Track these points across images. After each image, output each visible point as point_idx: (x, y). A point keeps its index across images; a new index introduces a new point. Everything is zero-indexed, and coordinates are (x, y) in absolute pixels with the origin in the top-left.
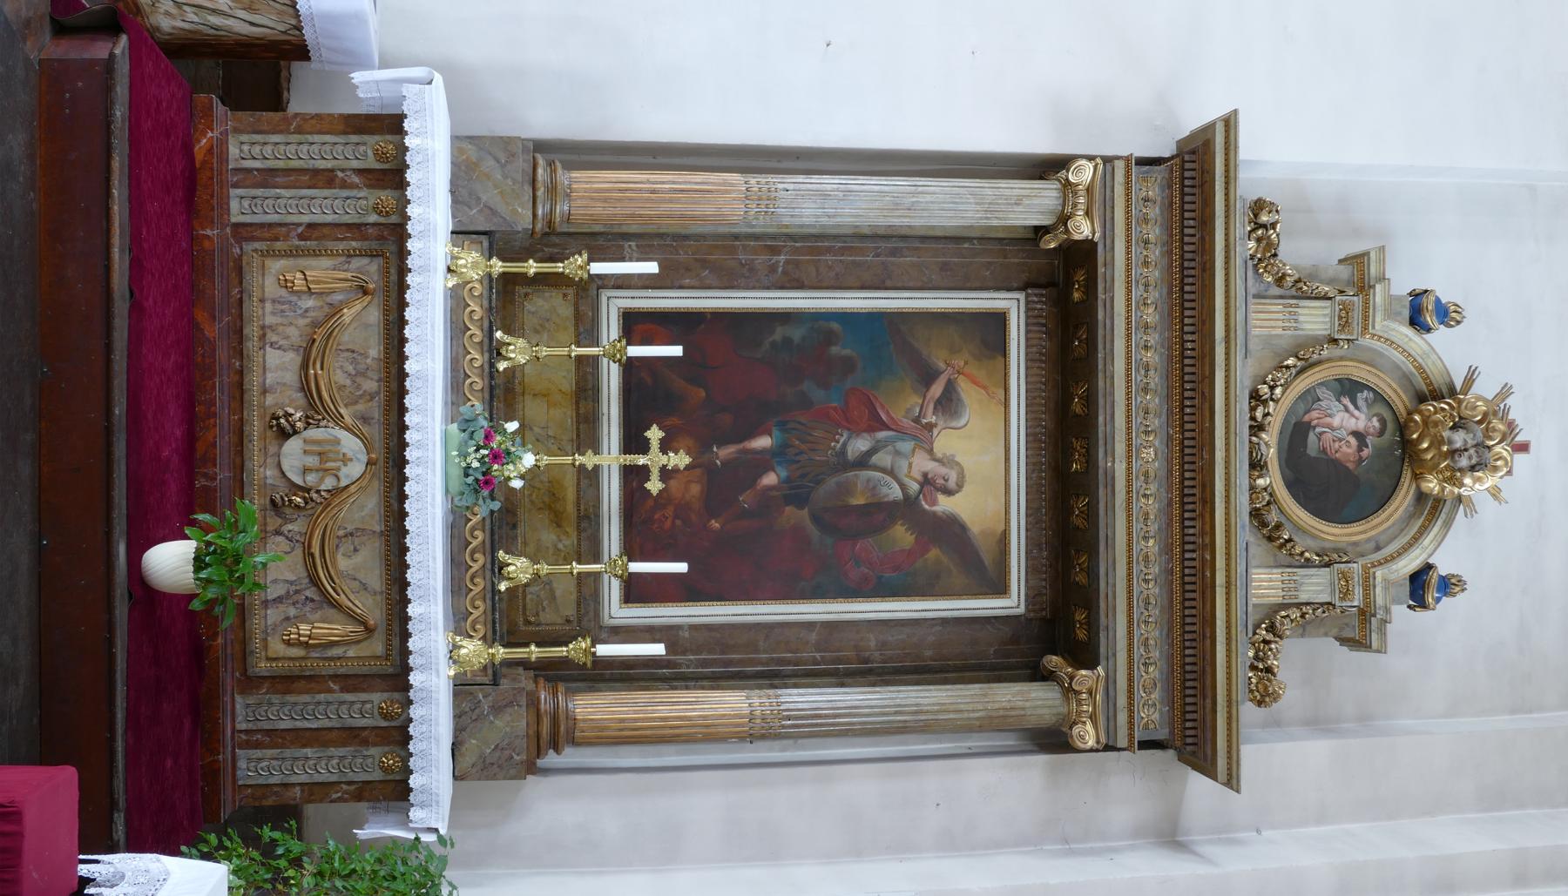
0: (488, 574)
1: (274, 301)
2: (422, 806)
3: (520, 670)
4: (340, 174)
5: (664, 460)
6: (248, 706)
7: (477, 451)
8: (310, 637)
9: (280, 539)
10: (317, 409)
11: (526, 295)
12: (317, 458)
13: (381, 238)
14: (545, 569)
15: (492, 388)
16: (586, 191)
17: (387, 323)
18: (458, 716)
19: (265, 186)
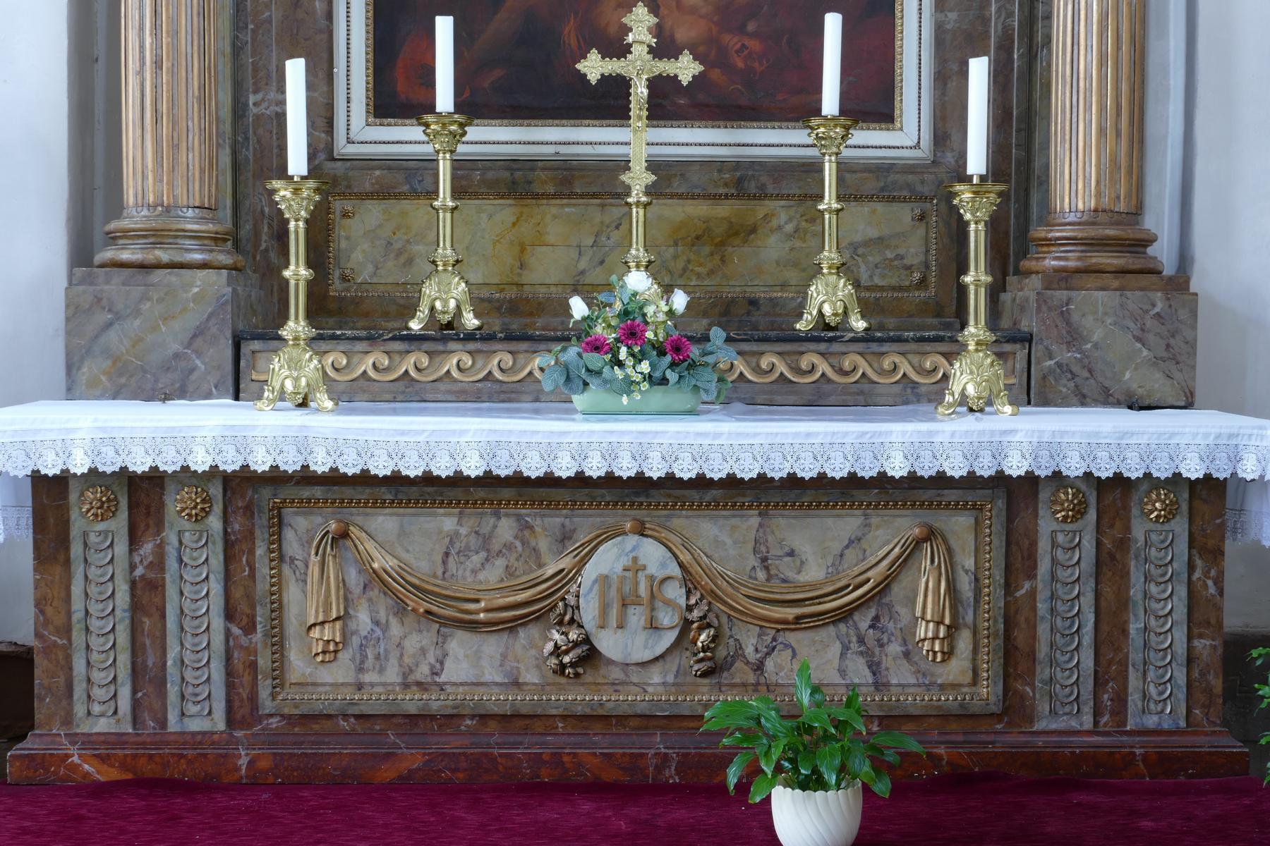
0: (836, 347)
1: (361, 670)
2: (1236, 459)
3: (1005, 297)
4: (139, 571)
5: (639, 51)
6: (1053, 712)
7: (621, 364)
8: (939, 623)
9: (769, 665)
10: (549, 606)
11: (344, 279)
12: (631, 610)
13: (249, 510)
14: (829, 255)
15: (510, 338)
16: (158, 180)
17: (396, 503)
18: (1083, 400)
19: (161, 683)
